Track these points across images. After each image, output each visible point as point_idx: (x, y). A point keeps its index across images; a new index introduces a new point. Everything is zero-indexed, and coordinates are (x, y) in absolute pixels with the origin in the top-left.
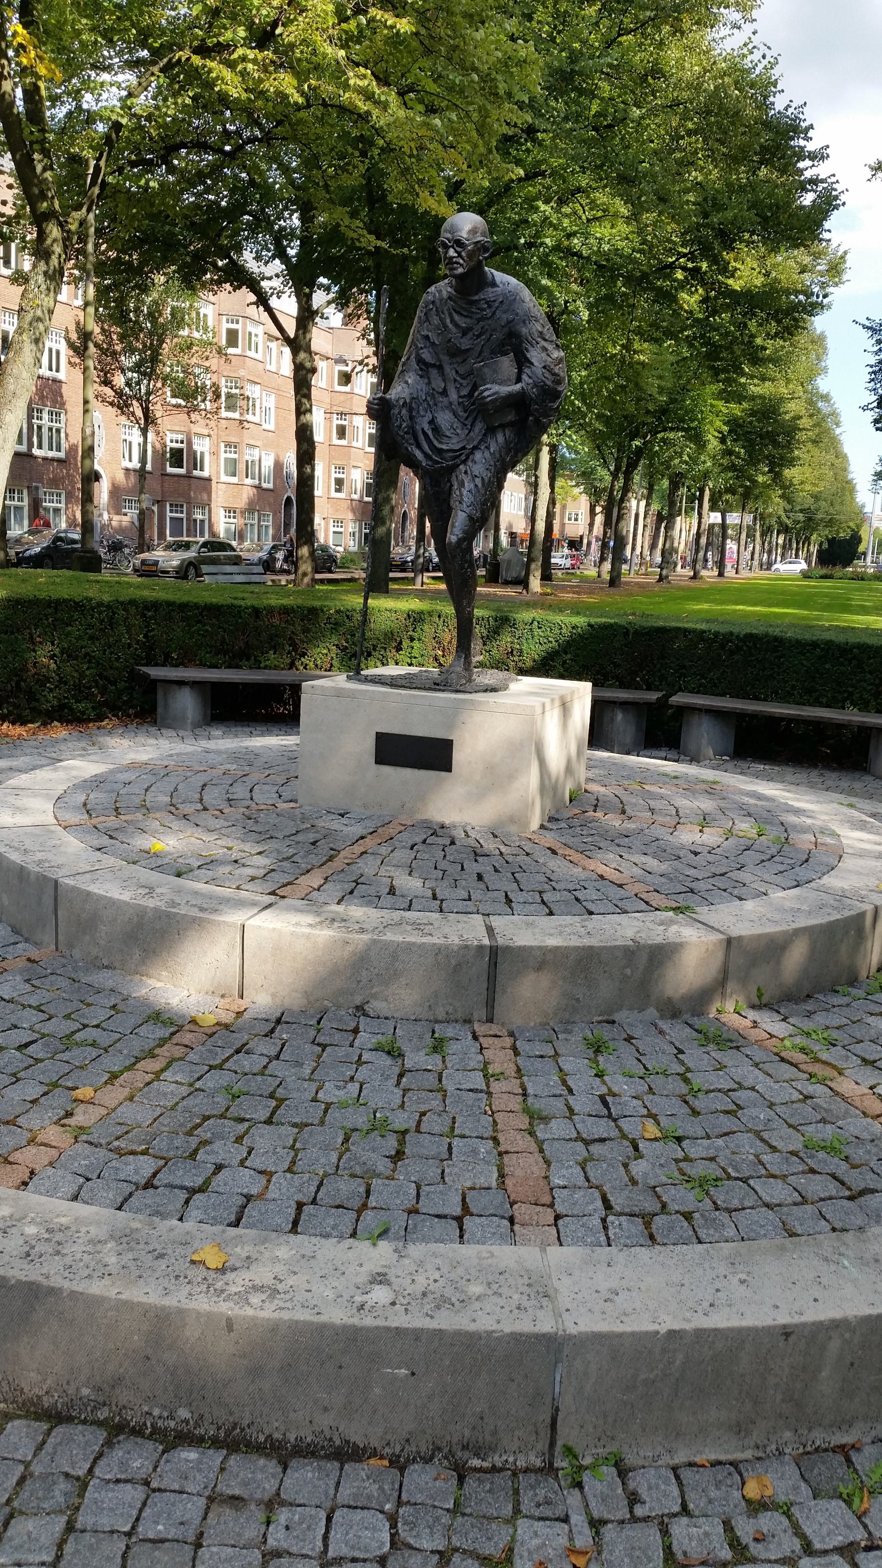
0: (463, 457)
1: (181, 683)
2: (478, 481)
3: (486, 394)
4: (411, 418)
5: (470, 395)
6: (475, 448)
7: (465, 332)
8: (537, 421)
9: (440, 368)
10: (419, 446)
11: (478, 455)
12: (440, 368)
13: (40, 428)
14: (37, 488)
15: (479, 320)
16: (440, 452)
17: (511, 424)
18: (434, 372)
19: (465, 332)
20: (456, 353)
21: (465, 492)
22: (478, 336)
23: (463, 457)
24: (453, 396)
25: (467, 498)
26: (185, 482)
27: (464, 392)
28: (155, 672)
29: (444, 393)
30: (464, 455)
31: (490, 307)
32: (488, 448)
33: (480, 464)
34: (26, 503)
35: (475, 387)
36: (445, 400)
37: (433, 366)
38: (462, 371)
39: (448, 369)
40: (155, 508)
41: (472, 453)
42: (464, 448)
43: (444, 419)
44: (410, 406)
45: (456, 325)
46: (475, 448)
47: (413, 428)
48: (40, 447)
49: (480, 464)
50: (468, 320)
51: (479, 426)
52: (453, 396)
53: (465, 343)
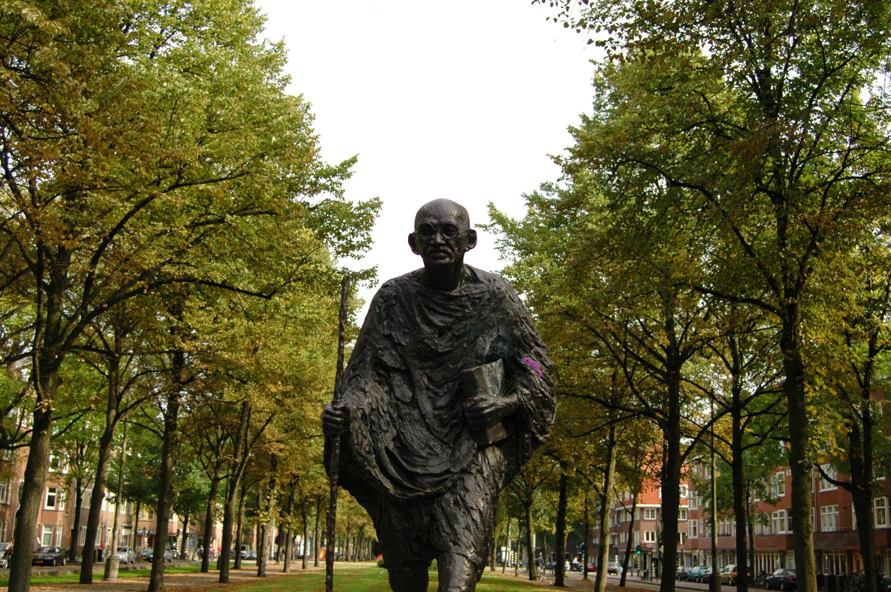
5: (449, 407)
15: (459, 320)
18: (397, 379)
19: (441, 332)
29: (414, 403)
30: (452, 482)
37: (395, 370)
39: (417, 374)
42: (448, 471)
45: (431, 324)
50: (447, 319)
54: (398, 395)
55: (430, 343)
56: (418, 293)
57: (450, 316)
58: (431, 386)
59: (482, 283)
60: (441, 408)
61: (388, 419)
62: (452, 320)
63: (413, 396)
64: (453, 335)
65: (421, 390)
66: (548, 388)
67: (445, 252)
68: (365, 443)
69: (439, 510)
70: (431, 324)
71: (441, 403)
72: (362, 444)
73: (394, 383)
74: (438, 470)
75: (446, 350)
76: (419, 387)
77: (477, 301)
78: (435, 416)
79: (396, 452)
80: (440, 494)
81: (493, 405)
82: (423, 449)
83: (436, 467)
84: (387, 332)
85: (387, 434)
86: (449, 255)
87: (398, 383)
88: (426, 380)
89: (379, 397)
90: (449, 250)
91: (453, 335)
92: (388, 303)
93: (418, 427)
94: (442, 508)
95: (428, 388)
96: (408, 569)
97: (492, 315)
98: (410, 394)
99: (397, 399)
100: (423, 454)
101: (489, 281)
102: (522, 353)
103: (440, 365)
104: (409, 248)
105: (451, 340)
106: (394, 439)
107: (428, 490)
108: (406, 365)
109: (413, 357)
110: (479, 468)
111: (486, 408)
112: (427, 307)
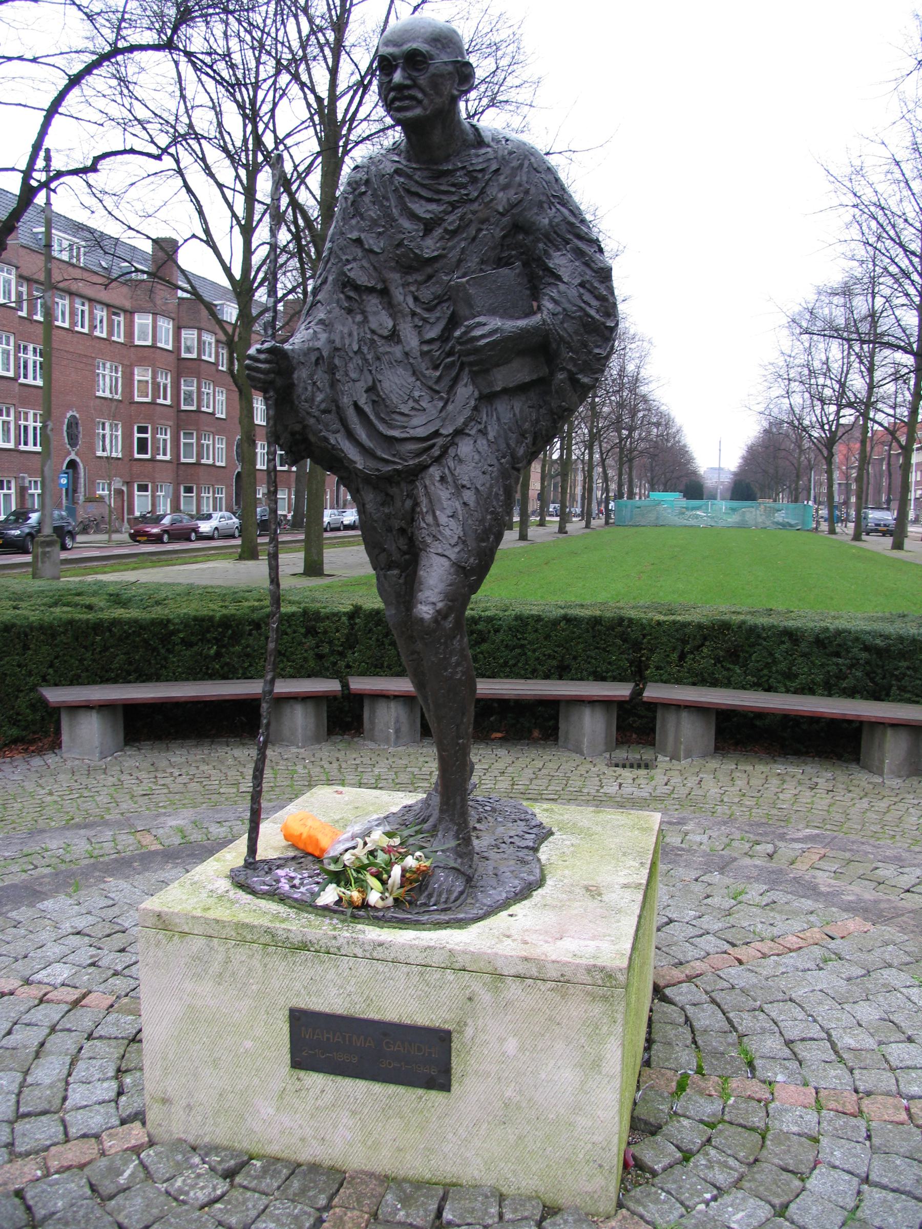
0: (436, 452)
1: (87, 707)
2: (469, 496)
3: (477, 333)
4: (333, 384)
5: (444, 337)
6: (459, 433)
7: (429, 226)
8: (573, 381)
9: (384, 293)
10: (351, 435)
11: (465, 448)
12: (384, 293)
13: (26, 428)
14: (23, 478)
15: (454, 206)
16: (391, 441)
17: (522, 389)
18: (373, 303)
19: (429, 226)
20: (413, 265)
21: (443, 519)
22: (454, 233)
23: (436, 452)
24: (412, 341)
25: (451, 529)
26: (150, 464)
27: (433, 333)
28: (54, 695)
29: (394, 336)
30: (437, 449)
31: (474, 181)
32: (483, 432)
33: (472, 460)
34: (13, 491)
35: (453, 321)
36: (397, 351)
37: (371, 290)
38: (426, 294)
39: (398, 294)
40: (125, 489)
41: (453, 444)
42: (436, 434)
43: (396, 383)
44: (326, 361)
45: (413, 216)
46: (459, 433)
47: (335, 401)
48: (26, 444)
49: (472, 460)
50: (433, 207)
51: (465, 392)
52: (412, 341)
53: (430, 247)
54: (374, 326)
55: (412, 245)
56: (397, 171)
57: (438, 201)
58: (418, 310)
59: (488, 146)
60: (430, 342)
61: (360, 362)
62: (442, 208)
63: (394, 326)
64: (446, 231)
65: (404, 316)
66: (594, 303)
67: (413, 98)
68: (320, 397)
69: (421, 491)
70: (413, 216)
71: (432, 333)
72: (313, 400)
73: (368, 309)
74: (421, 432)
75: (436, 254)
76: (401, 311)
77: (480, 176)
78: (423, 354)
79: (368, 409)
80: (424, 467)
81: (495, 331)
82: (406, 402)
83: (419, 426)
84: (354, 235)
85: (358, 384)
86: (420, 102)
87: (375, 309)
88: (410, 300)
89: (346, 331)
90: (420, 96)
91: (446, 231)
92: (357, 193)
93: (400, 371)
94: (425, 487)
95: (414, 314)
96: (396, 572)
97: (501, 195)
98: (390, 324)
99: (373, 332)
100: (405, 409)
101: (499, 142)
102: (551, 251)
103: (430, 277)
104: (591, 188)
105: (442, 238)
106: (368, 390)
107: (411, 463)
108: (384, 281)
109: (393, 269)
110: (480, 427)
111: (483, 336)
112: (408, 191)
